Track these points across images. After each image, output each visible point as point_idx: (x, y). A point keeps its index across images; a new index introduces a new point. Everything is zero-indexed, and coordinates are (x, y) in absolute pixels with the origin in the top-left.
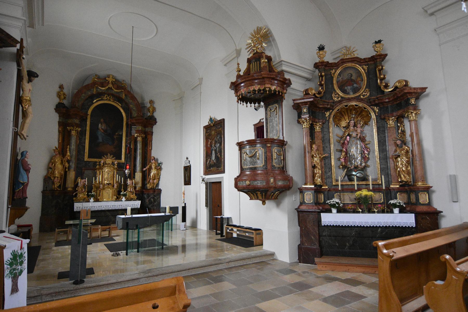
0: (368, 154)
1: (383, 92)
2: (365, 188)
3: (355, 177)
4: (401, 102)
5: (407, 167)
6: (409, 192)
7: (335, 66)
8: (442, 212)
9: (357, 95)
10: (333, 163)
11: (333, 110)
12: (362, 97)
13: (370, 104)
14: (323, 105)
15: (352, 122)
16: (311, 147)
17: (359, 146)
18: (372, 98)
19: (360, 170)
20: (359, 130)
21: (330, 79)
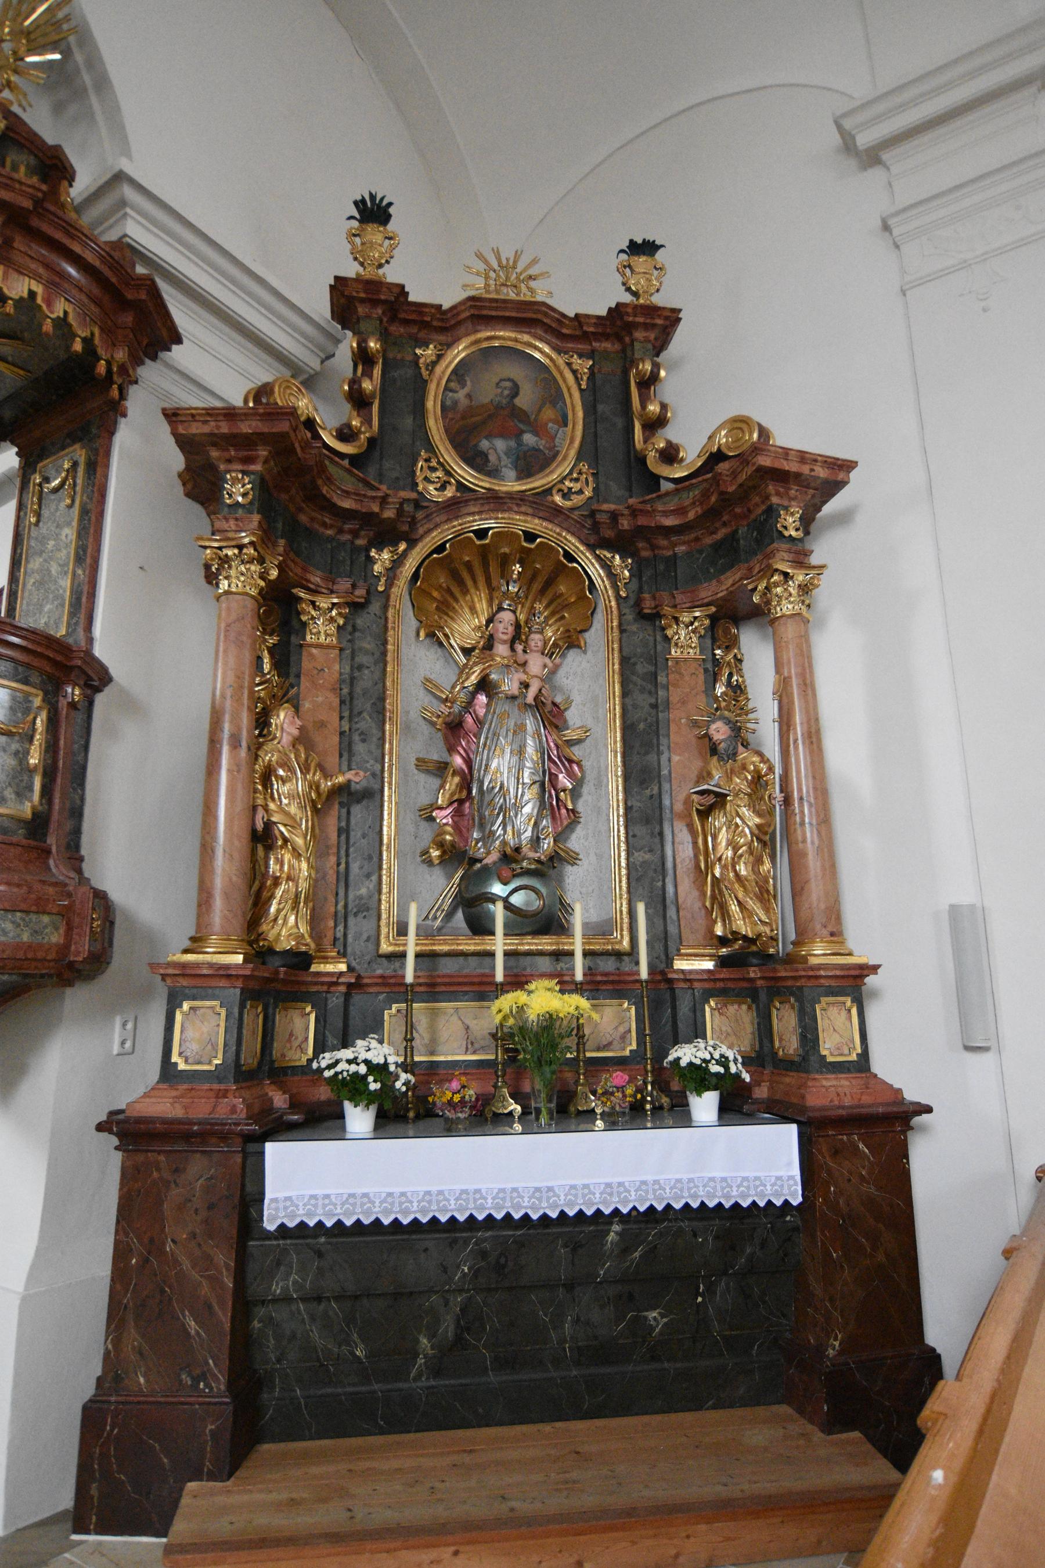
0: (575, 793)
1: (655, 479)
2: (550, 976)
3: (498, 911)
4: (731, 531)
5: (759, 861)
6: (763, 996)
7: (439, 323)
8: (929, 1110)
9: (538, 483)
10: (388, 830)
11: (412, 543)
12: (558, 499)
13: (592, 540)
14: (359, 497)
15: (506, 616)
16: (262, 722)
17: (531, 749)
18: (605, 507)
19: (527, 873)
20: (536, 664)
21: (406, 389)
